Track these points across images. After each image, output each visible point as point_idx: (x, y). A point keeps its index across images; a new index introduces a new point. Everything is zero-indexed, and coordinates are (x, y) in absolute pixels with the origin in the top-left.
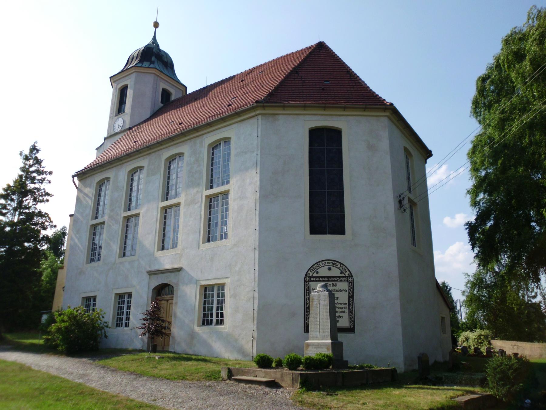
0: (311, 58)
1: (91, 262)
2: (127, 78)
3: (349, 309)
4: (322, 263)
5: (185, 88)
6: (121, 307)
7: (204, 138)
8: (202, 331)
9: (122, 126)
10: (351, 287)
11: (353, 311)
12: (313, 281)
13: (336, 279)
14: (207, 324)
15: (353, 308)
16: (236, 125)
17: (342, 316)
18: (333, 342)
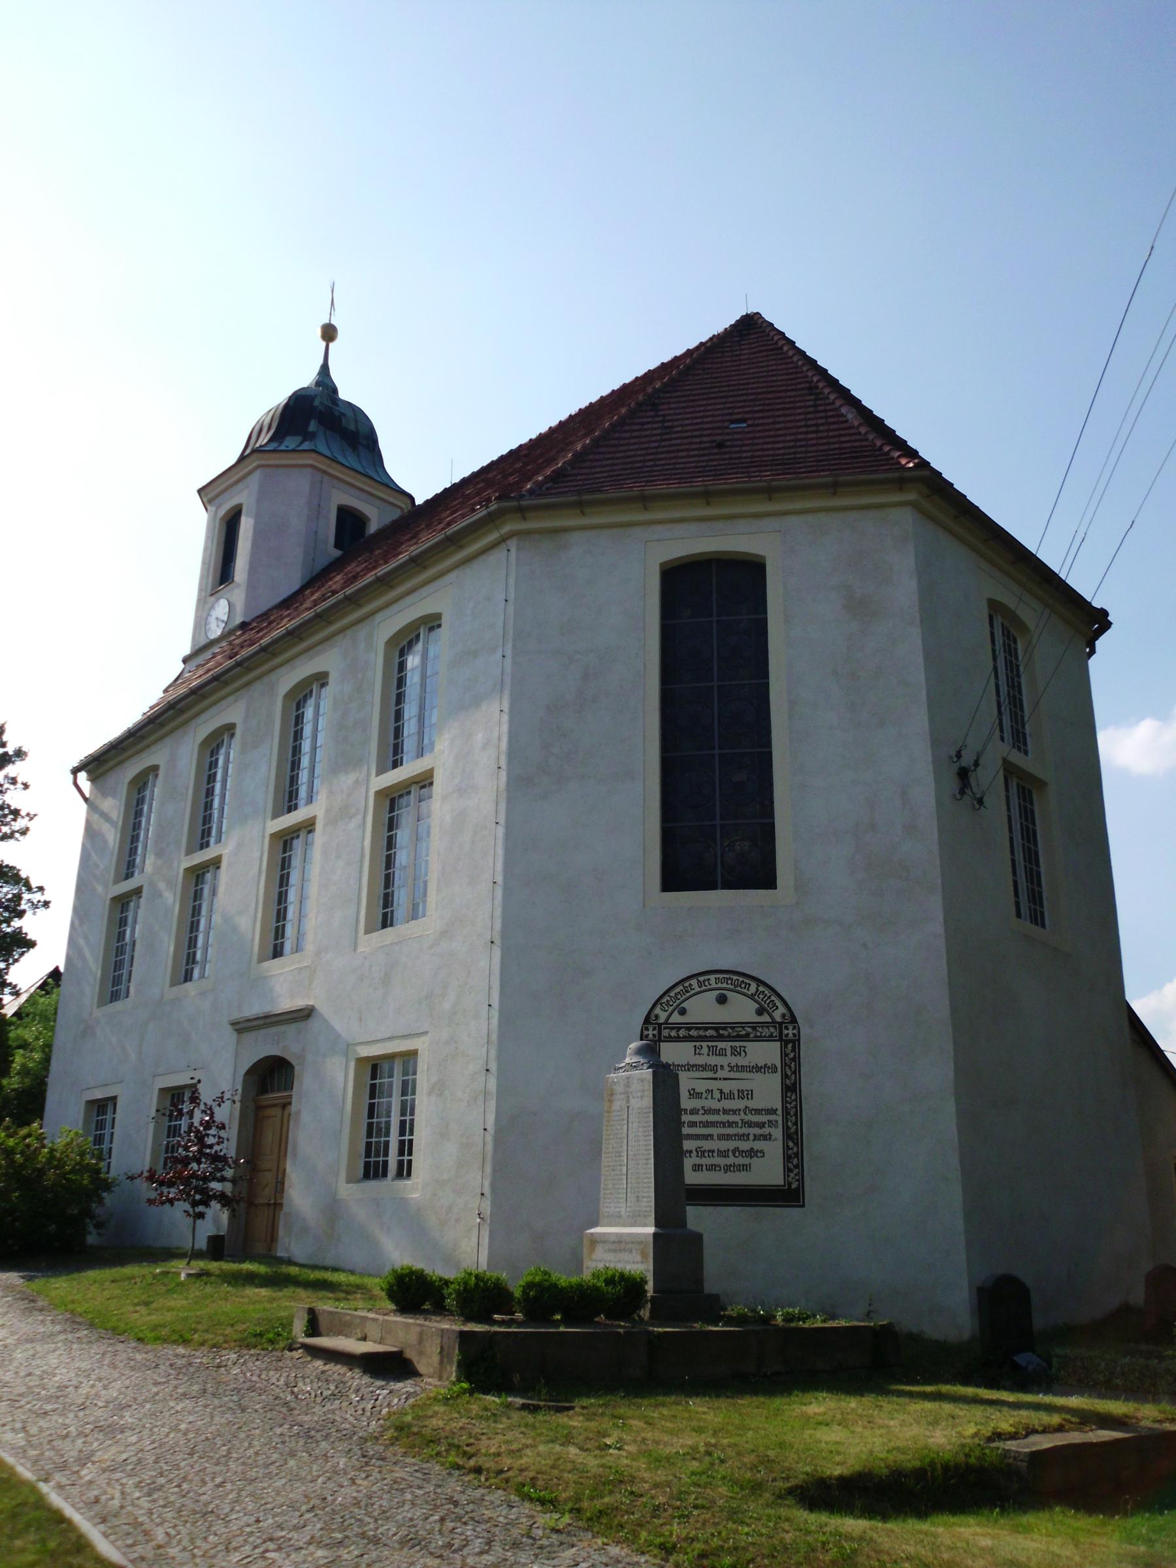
0: (708, 364)
1: (111, 1002)
2: (240, 486)
3: (786, 1129)
4: (699, 981)
5: (409, 501)
6: (175, 1125)
7: (376, 623)
8: (352, 1193)
9: (225, 619)
10: (792, 1055)
11: (796, 1132)
12: (670, 1039)
13: (743, 1033)
14: (376, 1176)
15: (799, 1122)
16: (452, 576)
17: (762, 1152)
18: (659, 1230)
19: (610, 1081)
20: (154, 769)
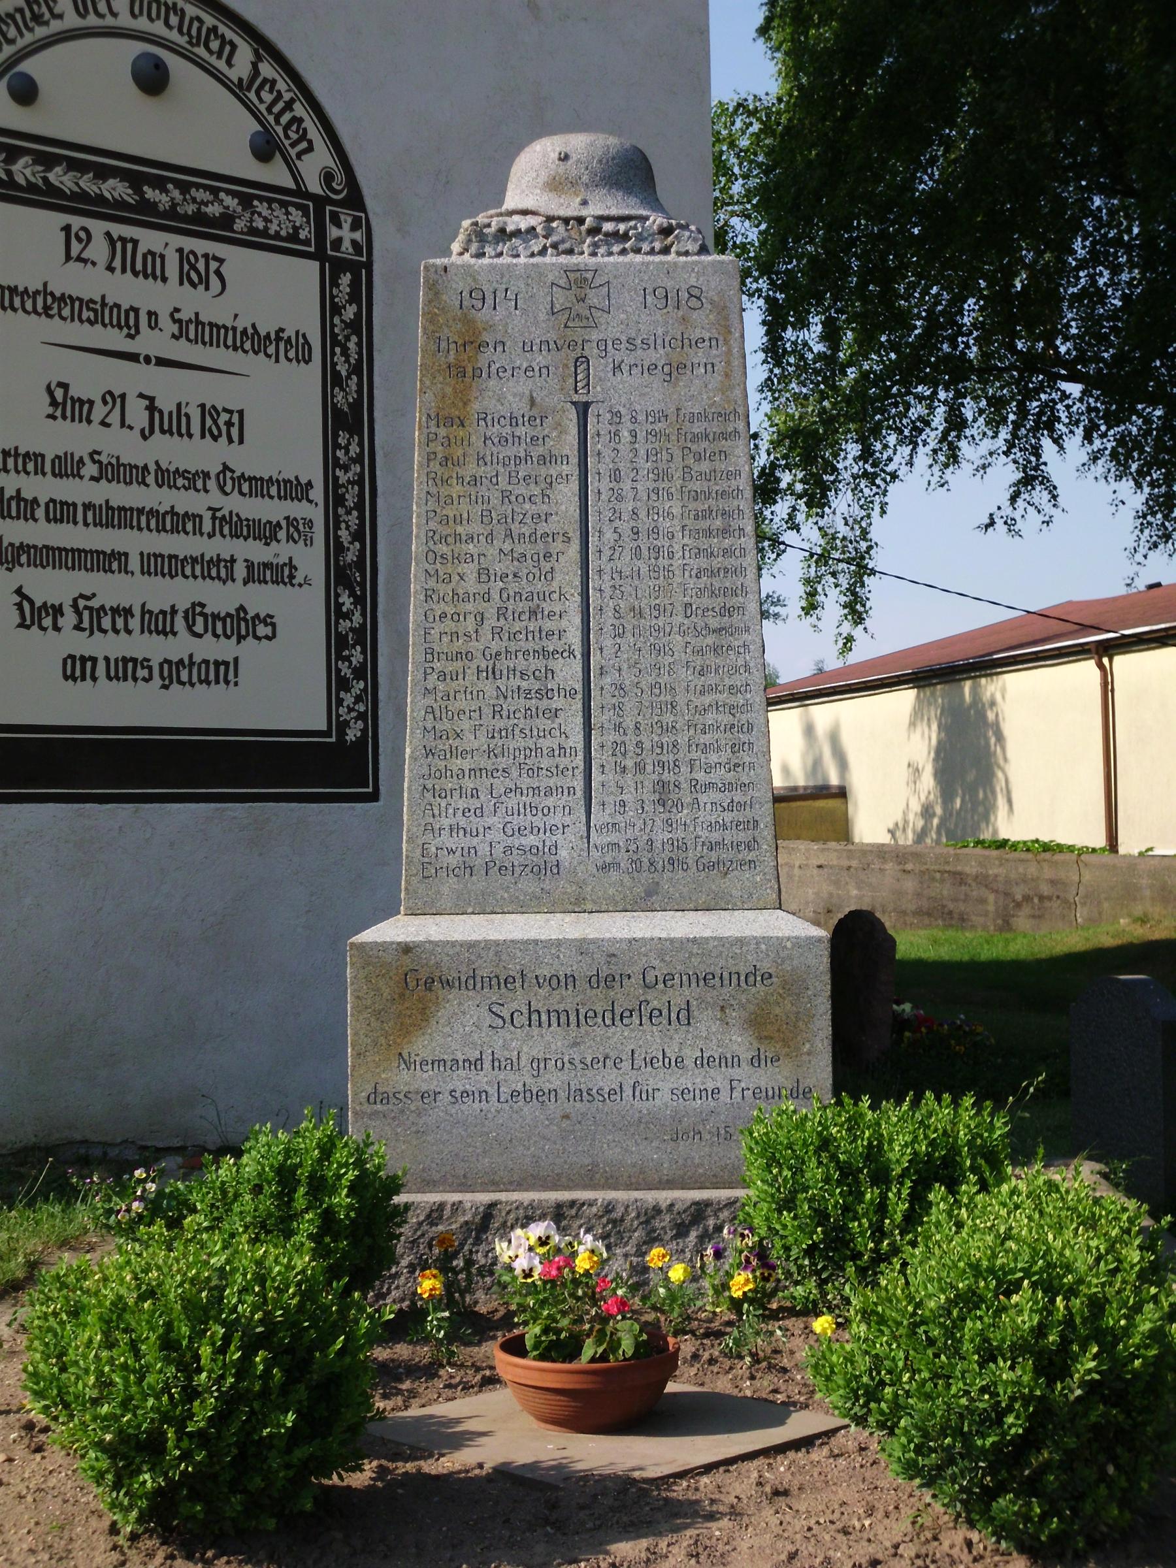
3: (334, 549)
10: (350, 312)
11: (360, 563)
13: (214, 210)
17: (268, 621)
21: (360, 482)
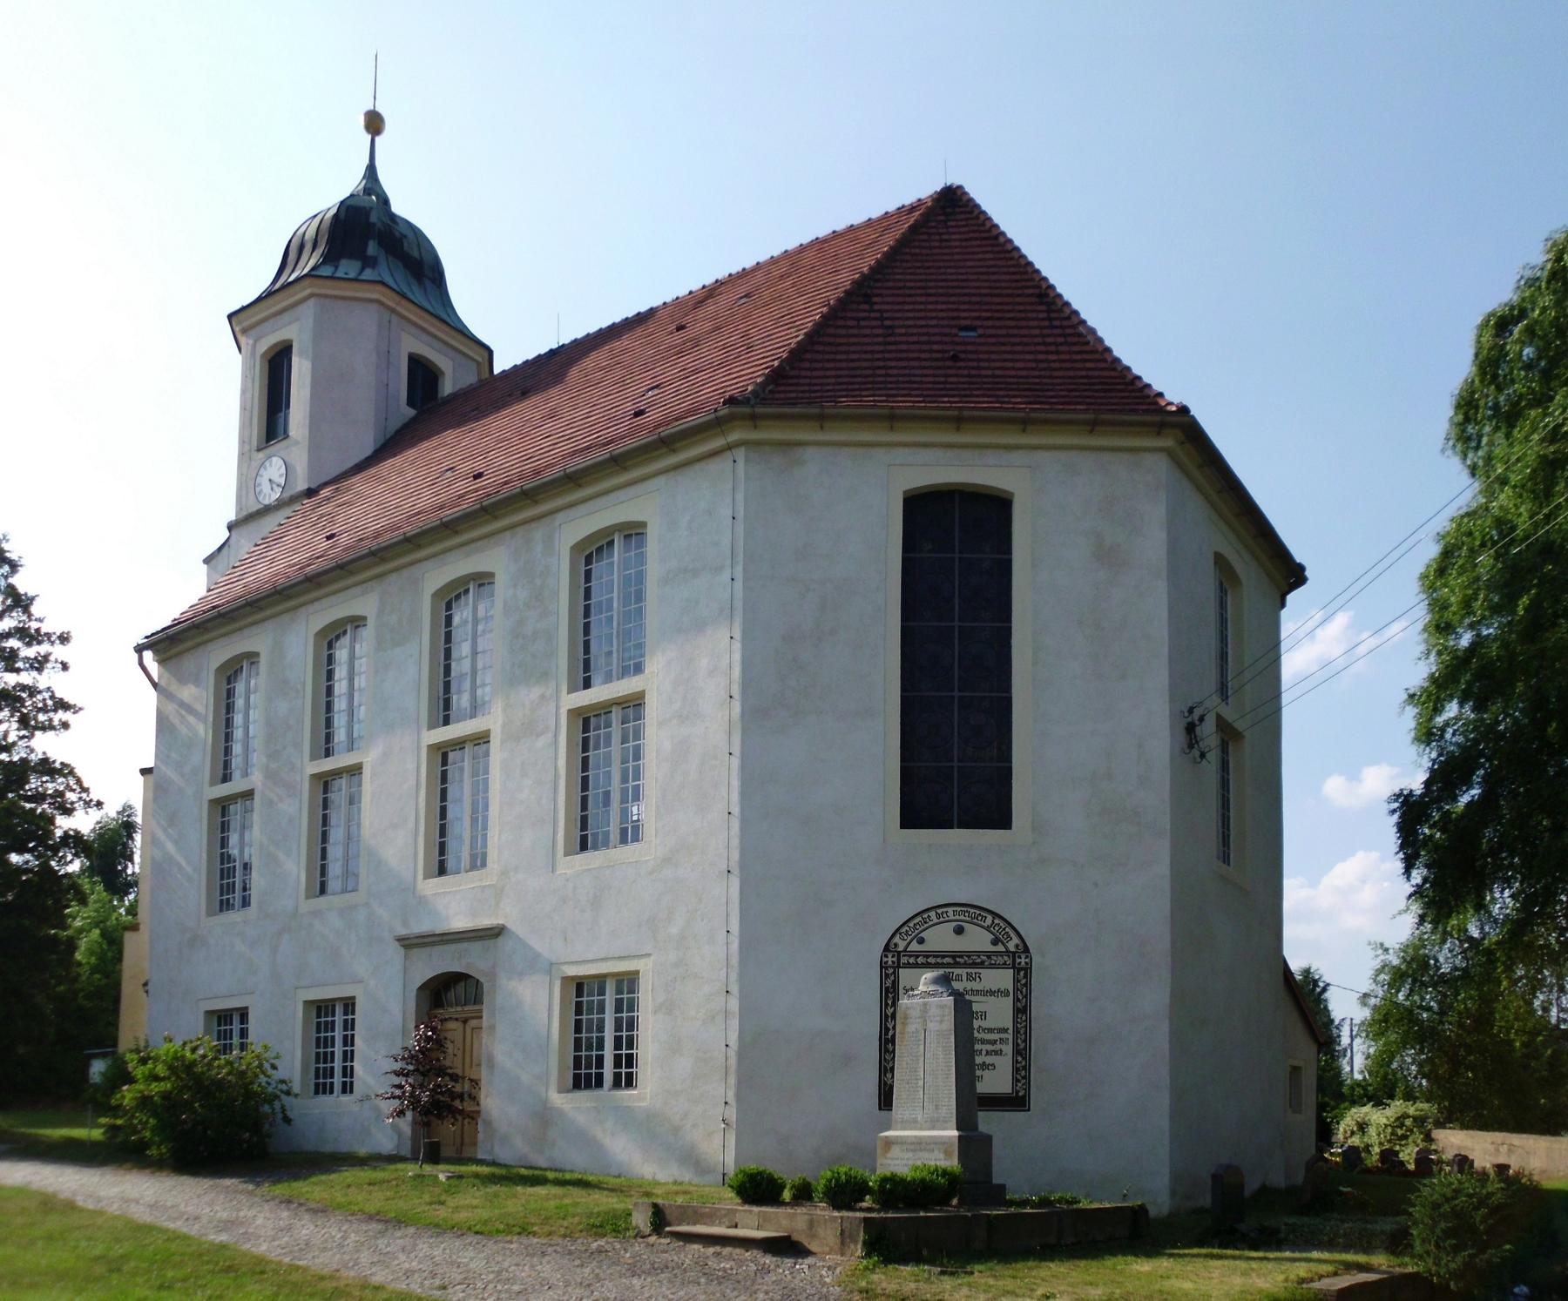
2: (286, 317)
3: (1016, 1045)
4: (937, 913)
5: (486, 354)
7: (557, 524)
10: (1024, 981)
11: (1025, 1048)
12: (908, 966)
13: (979, 961)
14: (588, 1086)
15: (1027, 1040)
16: (660, 481)
17: (993, 1065)
19: (904, 1006)
20: (252, 657)
21: (1026, 1027)
